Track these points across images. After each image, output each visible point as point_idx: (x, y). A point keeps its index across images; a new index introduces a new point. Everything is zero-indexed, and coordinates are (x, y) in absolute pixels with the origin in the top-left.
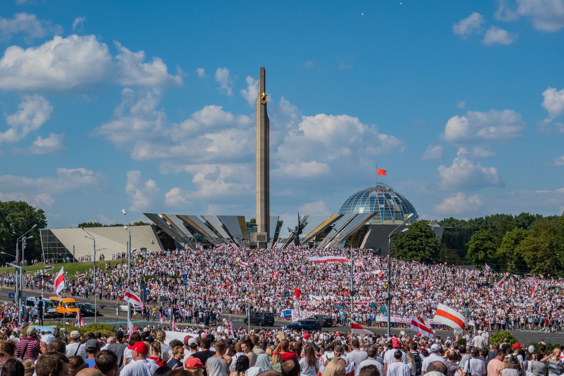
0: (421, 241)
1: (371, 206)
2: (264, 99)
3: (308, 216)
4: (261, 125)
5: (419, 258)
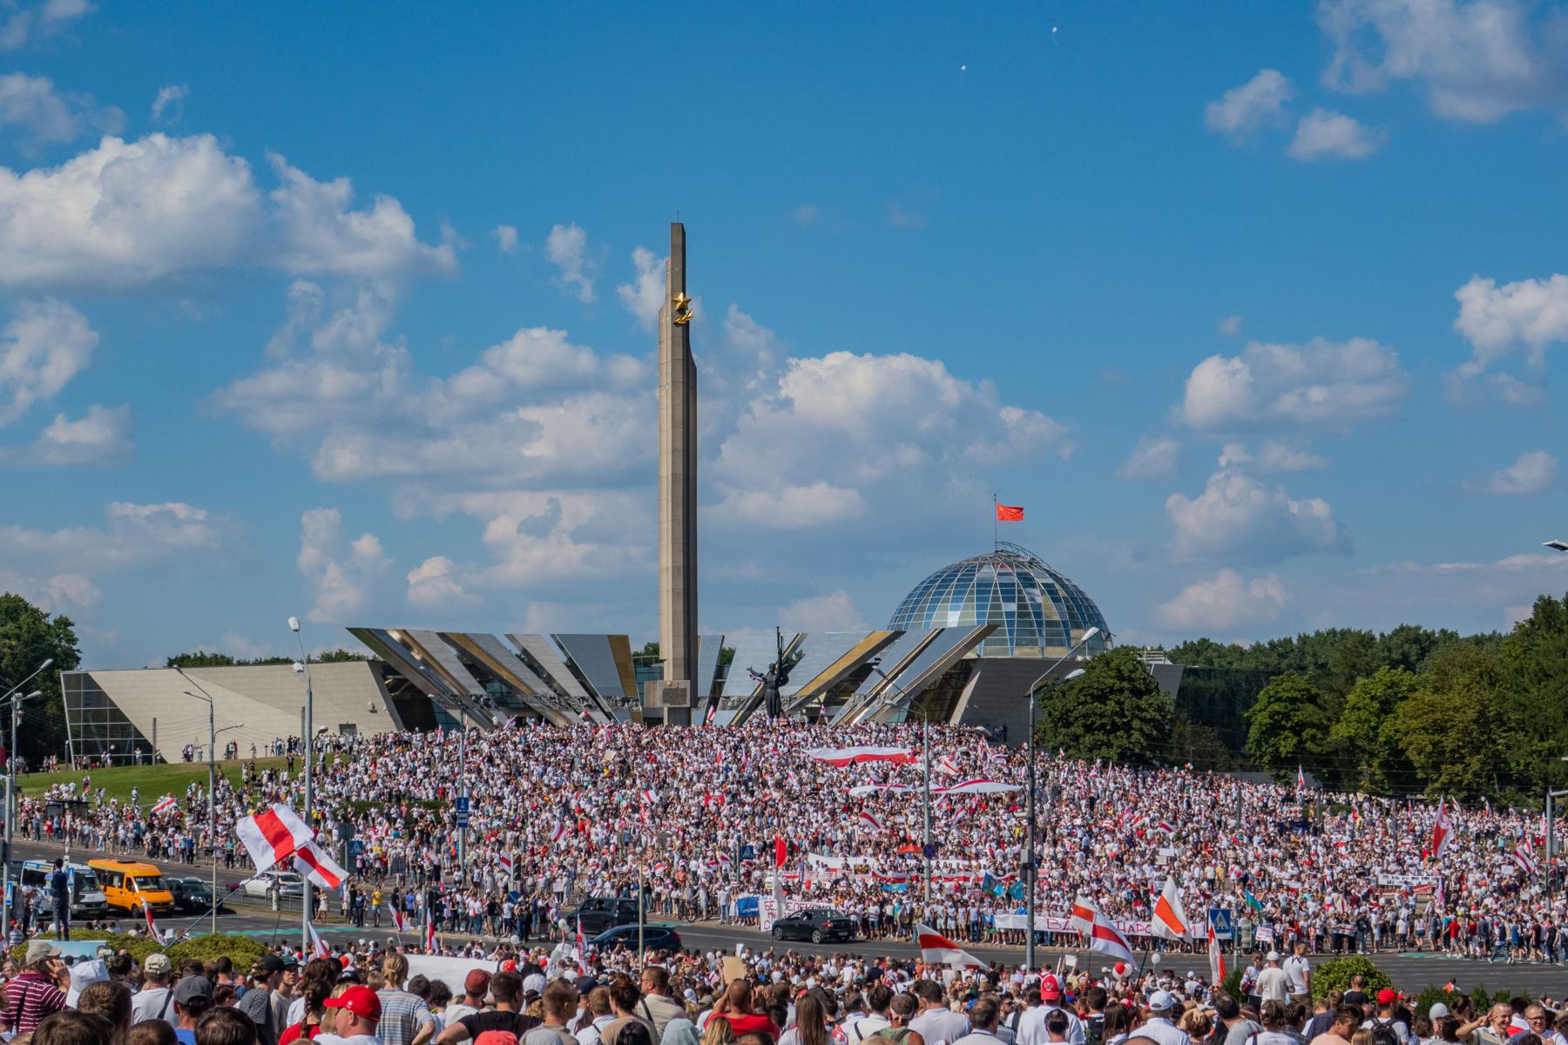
1: (979, 607)
2: (682, 310)
4: (674, 383)
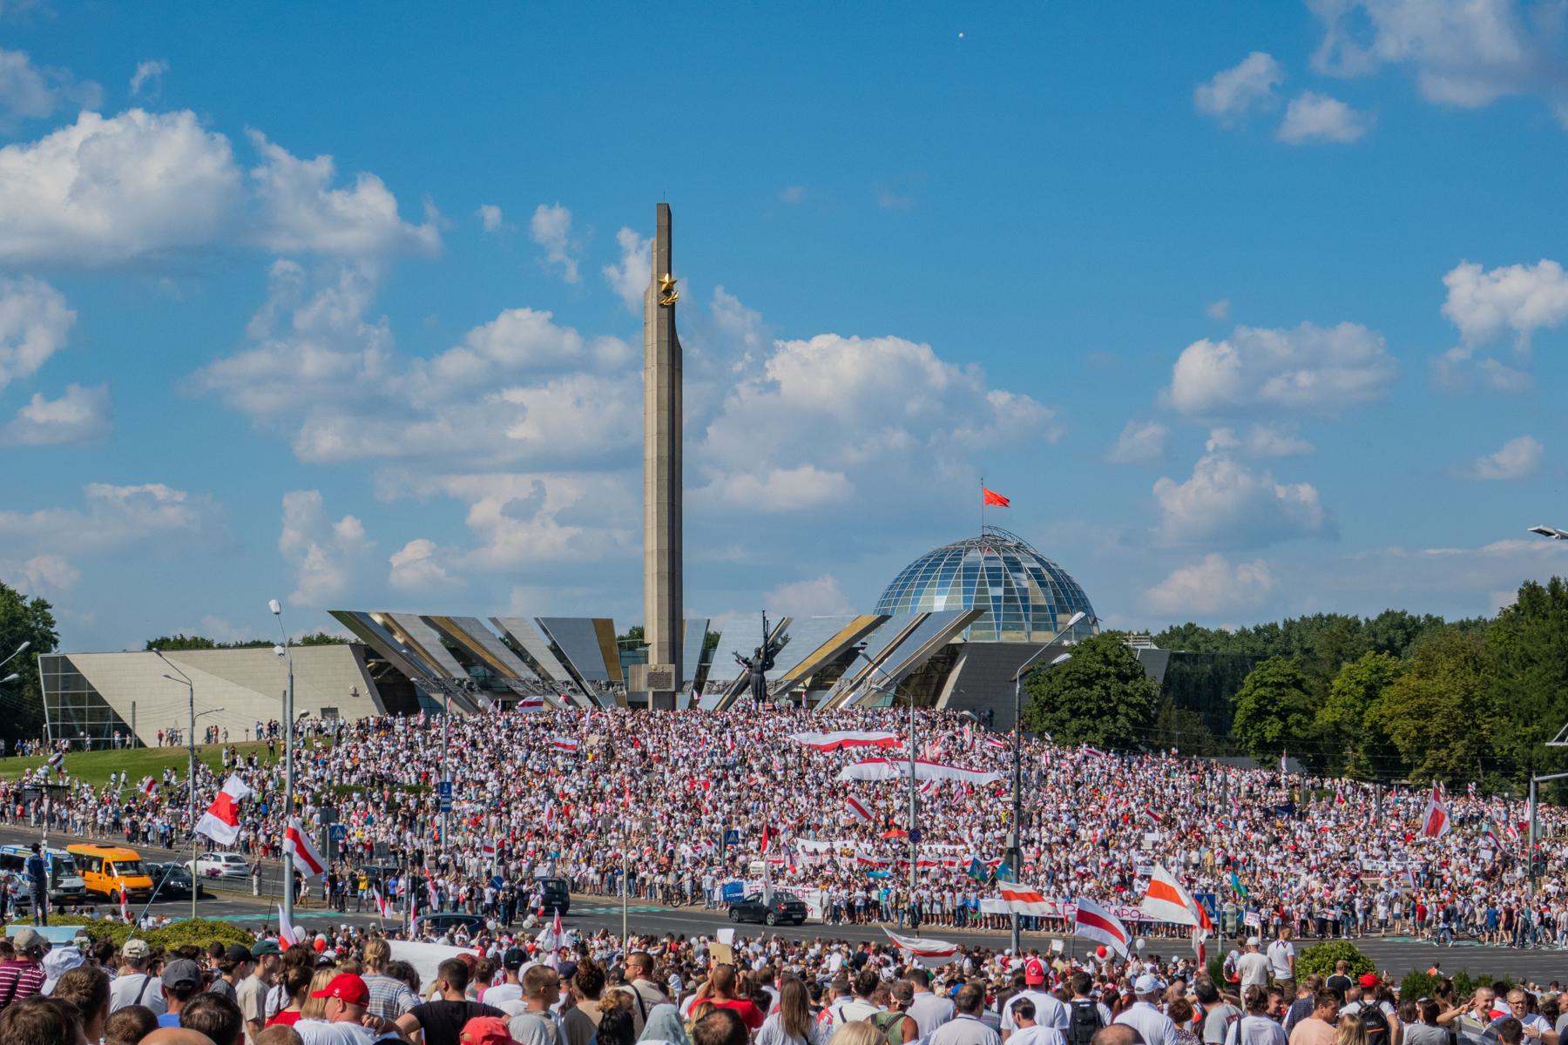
0: (1105, 688)
1: (965, 592)
2: (668, 292)
3: (790, 620)
4: (659, 365)
5: (1099, 738)
